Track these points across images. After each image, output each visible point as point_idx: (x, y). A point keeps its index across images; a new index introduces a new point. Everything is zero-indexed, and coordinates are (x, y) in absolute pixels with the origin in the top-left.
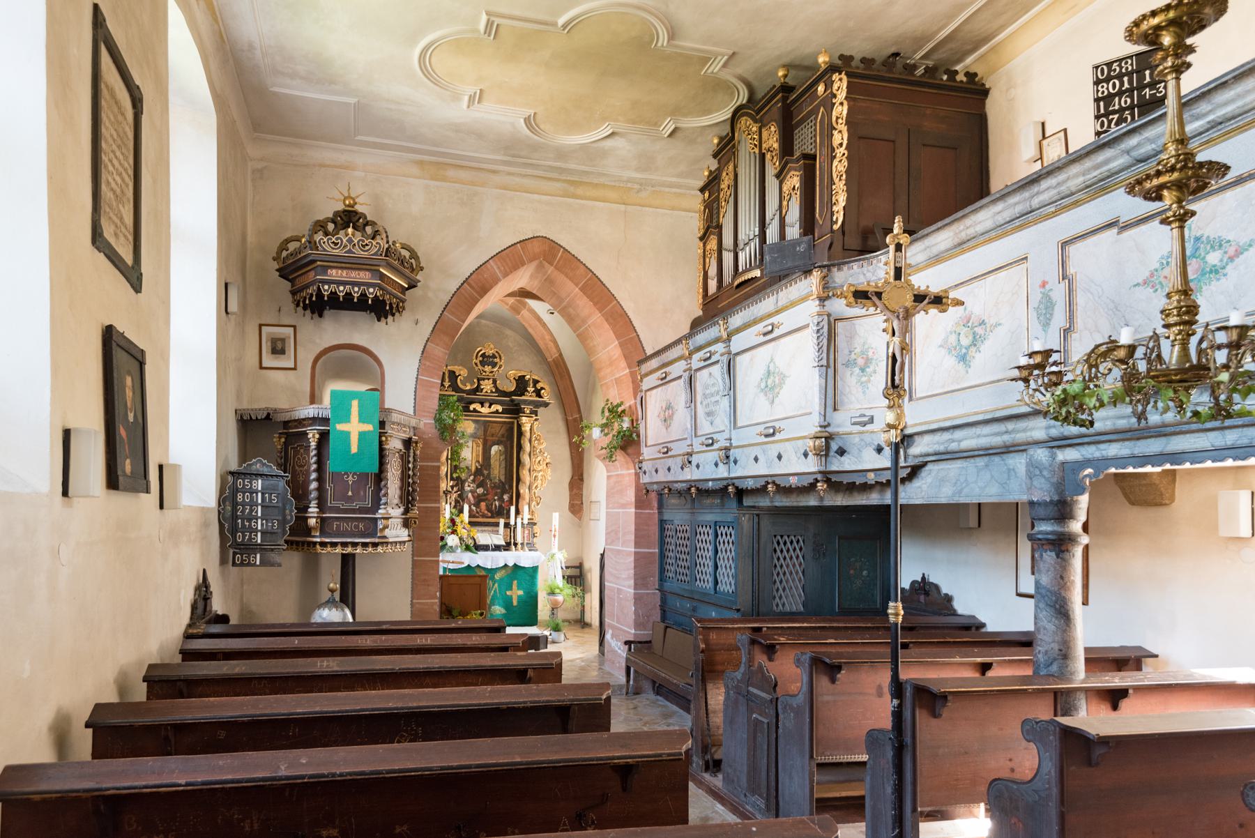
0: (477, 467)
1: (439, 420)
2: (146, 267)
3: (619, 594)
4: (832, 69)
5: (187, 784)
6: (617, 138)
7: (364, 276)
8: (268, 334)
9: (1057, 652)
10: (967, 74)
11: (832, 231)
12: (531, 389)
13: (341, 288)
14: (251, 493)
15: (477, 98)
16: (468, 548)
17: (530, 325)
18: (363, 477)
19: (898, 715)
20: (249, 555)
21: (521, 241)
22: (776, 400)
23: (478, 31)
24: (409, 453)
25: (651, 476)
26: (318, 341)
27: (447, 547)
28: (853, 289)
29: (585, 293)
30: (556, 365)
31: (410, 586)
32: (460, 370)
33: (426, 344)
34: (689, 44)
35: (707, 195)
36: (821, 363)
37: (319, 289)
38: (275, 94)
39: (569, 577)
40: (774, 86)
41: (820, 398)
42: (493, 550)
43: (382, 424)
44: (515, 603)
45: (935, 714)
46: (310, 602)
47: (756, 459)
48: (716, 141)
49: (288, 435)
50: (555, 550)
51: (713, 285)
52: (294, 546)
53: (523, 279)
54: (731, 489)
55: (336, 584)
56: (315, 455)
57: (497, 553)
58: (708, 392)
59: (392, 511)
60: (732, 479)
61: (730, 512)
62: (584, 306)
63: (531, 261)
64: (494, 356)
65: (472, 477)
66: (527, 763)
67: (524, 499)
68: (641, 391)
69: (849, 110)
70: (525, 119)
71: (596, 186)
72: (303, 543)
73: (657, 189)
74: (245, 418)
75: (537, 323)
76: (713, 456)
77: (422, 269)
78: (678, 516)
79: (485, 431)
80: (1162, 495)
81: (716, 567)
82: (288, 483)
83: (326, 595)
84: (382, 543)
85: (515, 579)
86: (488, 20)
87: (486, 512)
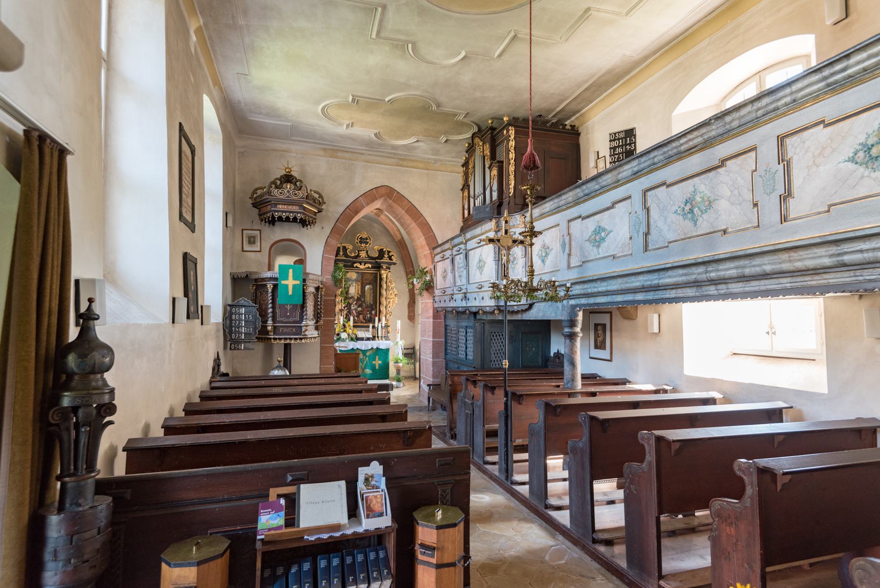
0: (358, 297)
1: (334, 277)
2: (196, 222)
3: (426, 361)
4: (509, 124)
5: (229, 422)
6: (420, 142)
7: (295, 208)
8: (246, 234)
9: (570, 379)
10: (571, 126)
11: (509, 197)
12: (386, 256)
13: (284, 214)
14: (239, 315)
15: (351, 125)
16: (352, 339)
17: (385, 223)
18: (295, 306)
19: (506, 404)
20: (238, 344)
21: (375, 188)
22: (483, 273)
23: (349, 101)
24: (318, 293)
25: (438, 304)
26: (272, 237)
27: (341, 339)
28: (488, 238)
29: (408, 214)
30: (400, 243)
31: (319, 359)
32: (349, 246)
33: (327, 239)
34: (447, 109)
35: (465, 169)
36: (496, 259)
37: (273, 214)
38: (250, 120)
39: (405, 354)
40: (488, 127)
41: (496, 274)
42: (366, 340)
43: (304, 280)
44: (377, 368)
45: (520, 404)
46: (268, 363)
47: (475, 299)
48: (467, 145)
49: (257, 286)
50: (398, 340)
51: (466, 215)
52: (260, 340)
53: (378, 204)
54: (467, 312)
55: (281, 358)
56: (271, 296)
57: (368, 342)
58: (459, 266)
59: (309, 323)
60: (468, 307)
61: (470, 323)
62: (408, 219)
63: (380, 197)
64: (367, 239)
65: (355, 302)
66: (348, 415)
67: (383, 313)
68: (434, 262)
69: (515, 144)
70: (374, 134)
71: (413, 161)
72: (265, 338)
73: (443, 162)
74: (235, 277)
75: (390, 222)
76: (460, 296)
77: (325, 203)
78: (452, 323)
79: (362, 278)
80: (632, 315)
81: (466, 348)
82: (257, 309)
83: (276, 364)
84: (304, 338)
85: (377, 355)
86: (353, 98)
87: (363, 320)
